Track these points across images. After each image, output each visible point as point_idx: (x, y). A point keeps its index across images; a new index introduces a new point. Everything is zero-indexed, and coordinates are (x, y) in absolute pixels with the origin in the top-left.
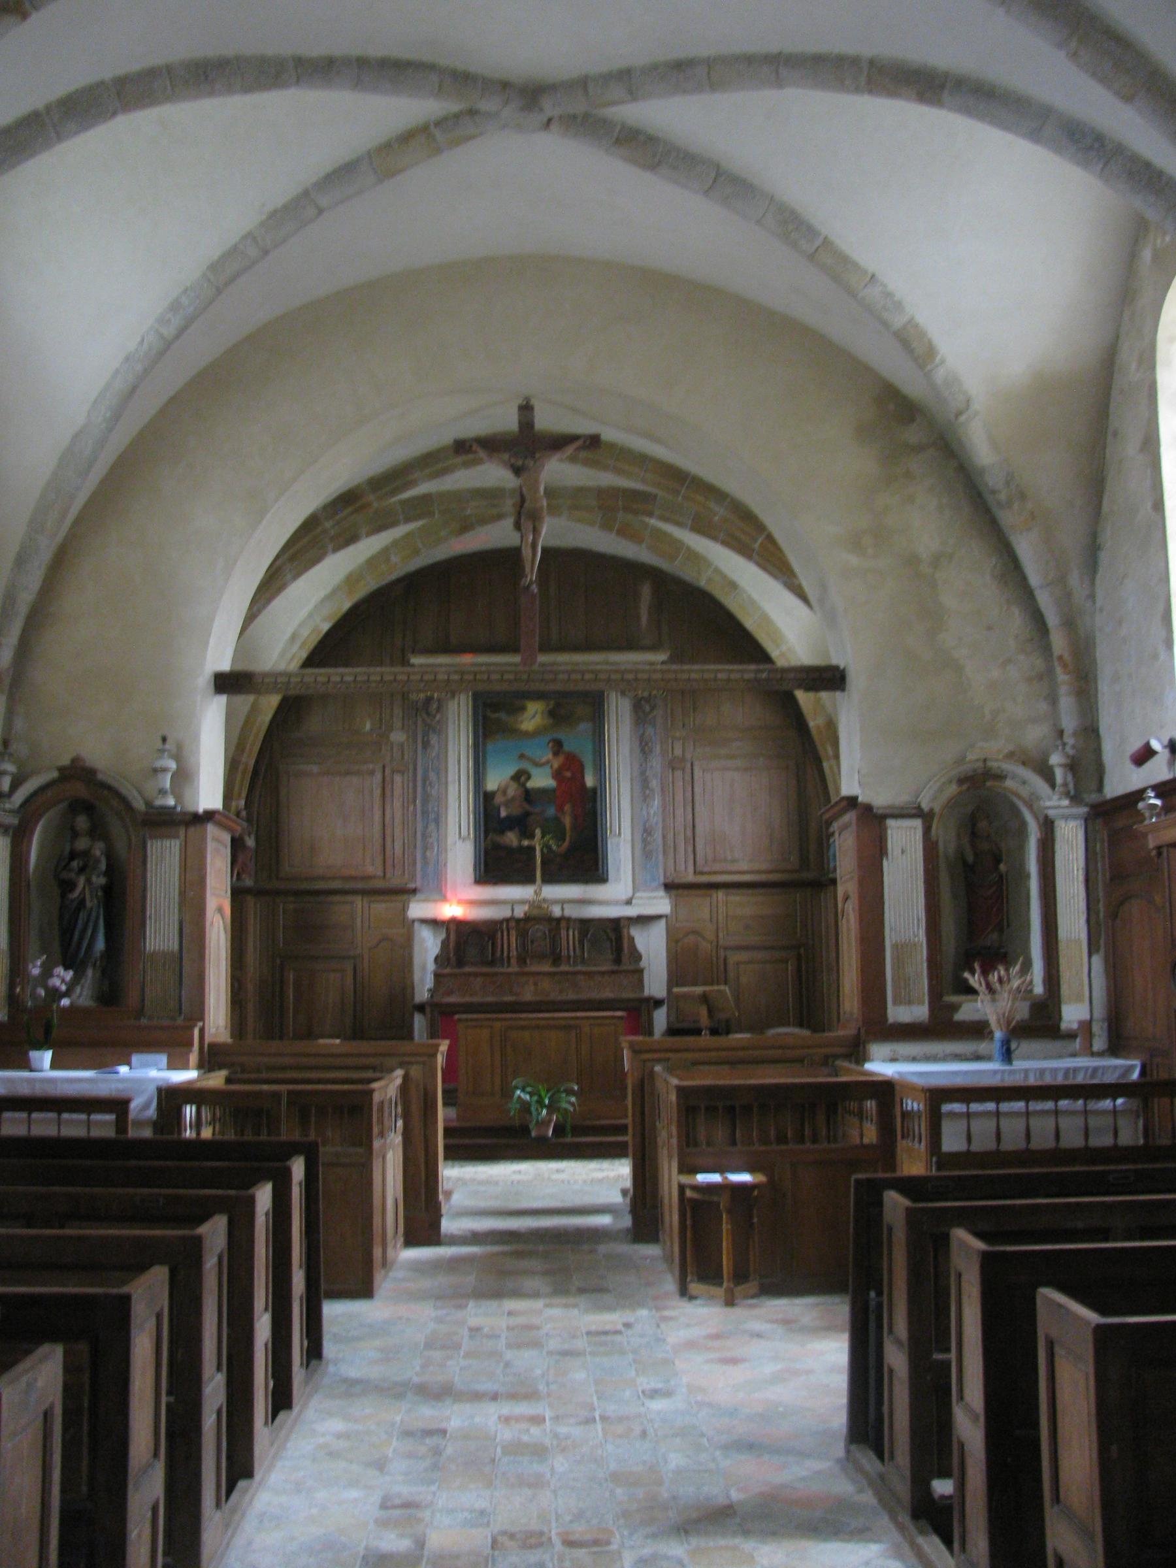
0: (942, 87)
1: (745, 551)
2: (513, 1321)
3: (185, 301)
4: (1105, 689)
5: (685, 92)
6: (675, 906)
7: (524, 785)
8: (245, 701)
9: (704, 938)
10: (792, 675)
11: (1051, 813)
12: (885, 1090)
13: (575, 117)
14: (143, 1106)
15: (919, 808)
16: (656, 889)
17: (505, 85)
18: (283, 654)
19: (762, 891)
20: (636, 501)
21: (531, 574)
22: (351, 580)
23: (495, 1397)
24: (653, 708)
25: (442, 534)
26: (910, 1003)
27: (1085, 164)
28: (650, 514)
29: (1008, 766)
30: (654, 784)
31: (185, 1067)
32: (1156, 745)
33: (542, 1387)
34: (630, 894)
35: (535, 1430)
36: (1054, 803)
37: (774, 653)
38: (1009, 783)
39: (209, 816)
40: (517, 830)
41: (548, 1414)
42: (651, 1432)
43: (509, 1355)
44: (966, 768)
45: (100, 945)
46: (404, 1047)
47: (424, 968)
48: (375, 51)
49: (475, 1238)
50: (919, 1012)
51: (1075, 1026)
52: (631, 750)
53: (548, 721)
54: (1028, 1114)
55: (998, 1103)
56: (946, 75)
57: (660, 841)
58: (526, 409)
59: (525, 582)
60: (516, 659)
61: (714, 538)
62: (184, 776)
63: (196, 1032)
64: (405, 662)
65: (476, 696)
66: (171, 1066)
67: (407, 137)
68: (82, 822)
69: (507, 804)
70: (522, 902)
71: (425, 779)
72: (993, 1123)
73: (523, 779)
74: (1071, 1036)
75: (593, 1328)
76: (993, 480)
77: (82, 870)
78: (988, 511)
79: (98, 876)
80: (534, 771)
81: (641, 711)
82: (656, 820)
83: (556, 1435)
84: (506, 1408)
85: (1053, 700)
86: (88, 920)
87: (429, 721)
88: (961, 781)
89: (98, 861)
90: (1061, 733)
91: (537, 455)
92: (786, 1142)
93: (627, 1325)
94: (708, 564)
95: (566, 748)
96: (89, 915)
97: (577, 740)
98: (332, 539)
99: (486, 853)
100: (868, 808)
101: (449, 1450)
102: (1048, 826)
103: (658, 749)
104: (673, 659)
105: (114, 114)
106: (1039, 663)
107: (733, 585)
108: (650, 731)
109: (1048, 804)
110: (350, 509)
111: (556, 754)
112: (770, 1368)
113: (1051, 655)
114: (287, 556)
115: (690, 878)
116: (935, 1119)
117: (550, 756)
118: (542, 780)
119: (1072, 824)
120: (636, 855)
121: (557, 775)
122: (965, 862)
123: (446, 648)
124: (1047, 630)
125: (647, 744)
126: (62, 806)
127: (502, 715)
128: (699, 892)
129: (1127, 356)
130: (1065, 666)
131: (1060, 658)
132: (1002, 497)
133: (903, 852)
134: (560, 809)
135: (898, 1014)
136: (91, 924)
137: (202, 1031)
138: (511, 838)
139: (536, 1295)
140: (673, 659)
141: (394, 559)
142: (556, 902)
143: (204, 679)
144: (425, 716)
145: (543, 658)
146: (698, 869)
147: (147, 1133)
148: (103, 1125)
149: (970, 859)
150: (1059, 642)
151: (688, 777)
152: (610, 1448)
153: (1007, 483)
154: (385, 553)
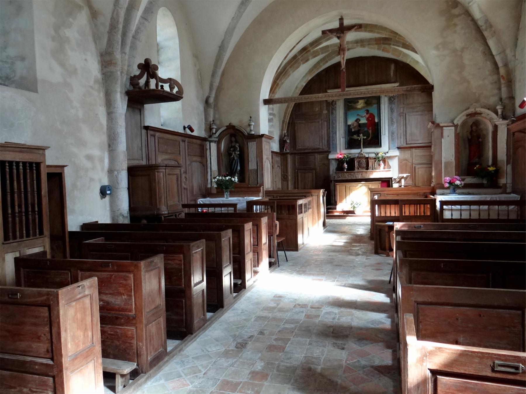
4: (518, 85)
6: (400, 153)
7: (358, 123)
9: (409, 162)
11: (497, 123)
16: (395, 149)
18: (294, 92)
24: (394, 99)
25: (333, 56)
30: (395, 120)
40: (357, 135)
45: (239, 168)
52: (388, 111)
53: (365, 105)
54: (470, 210)
55: (498, 206)
60: (340, 90)
62: (257, 125)
63: (262, 188)
64: (326, 92)
68: (233, 139)
69: (354, 128)
70: (357, 154)
71: (332, 122)
73: (358, 121)
79: (237, 152)
80: (361, 119)
81: (391, 100)
85: (500, 89)
86: (235, 163)
87: (333, 107)
92: (327, 213)
95: (370, 112)
96: (236, 162)
97: (373, 110)
98: (302, 60)
102: (496, 127)
103: (396, 111)
104: (400, 86)
108: (393, 106)
109: (495, 120)
111: (367, 114)
113: (500, 75)
115: (405, 145)
117: (365, 114)
118: (363, 121)
119: (503, 126)
120: (143, 151)
121: (368, 119)
122: (468, 139)
124: (499, 68)
125: (392, 110)
126: (229, 135)
128: (408, 149)
133: (448, 136)
134: (368, 128)
136: (236, 164)
137: (263, 188)
138: (355, 137)
140: (400, 86)
144: (331, 106)
145: (347, 89)
146: (407, 143)
148: (231, 210)
149: (470, 138)
150: (502, 71)
151: (404, 118)
153: (486, 23)
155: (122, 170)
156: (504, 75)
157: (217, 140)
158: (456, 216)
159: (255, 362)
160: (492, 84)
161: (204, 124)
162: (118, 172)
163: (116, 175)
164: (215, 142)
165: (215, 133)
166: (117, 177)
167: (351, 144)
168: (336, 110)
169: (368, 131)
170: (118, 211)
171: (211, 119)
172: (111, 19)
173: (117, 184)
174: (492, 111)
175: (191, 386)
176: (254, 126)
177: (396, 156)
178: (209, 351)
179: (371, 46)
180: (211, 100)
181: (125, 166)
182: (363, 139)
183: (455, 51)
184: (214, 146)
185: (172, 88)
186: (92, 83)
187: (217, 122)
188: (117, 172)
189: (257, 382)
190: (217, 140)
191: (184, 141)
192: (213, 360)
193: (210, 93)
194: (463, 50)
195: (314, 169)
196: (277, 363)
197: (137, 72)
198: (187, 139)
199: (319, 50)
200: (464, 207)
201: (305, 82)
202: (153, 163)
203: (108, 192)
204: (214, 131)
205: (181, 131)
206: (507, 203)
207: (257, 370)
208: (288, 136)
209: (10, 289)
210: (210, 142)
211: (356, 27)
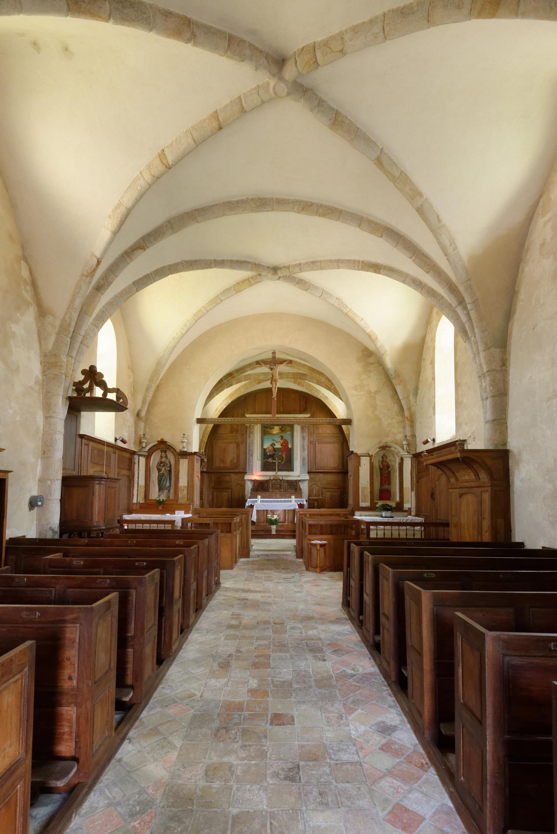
0: (380, 268)
1: (329, 389)
2: (266, 575)
3: (188, 324)
4: (418, 425)
5: (314, 270)
8: (204, 426)
10: (338, 421)
11: (403, 456)
12: (358, 522)
13: (286, 276)
14: (179, 524)
15: (369, 454)
16: (305, 473)
17: (268, 267)
19: (337, 474)
20: (302, 376)
21: (275, 395)
22: (231, 395)
23: (260, 592)
26: (365, 502)
27: (416, 290)
28: (306, 380)
29: (392, 444)
31: (189, 513)
32: (429, 440)
33: (271, 590)
34: (299, 474)
35: (269, 599)
36: (403, 453)
37: (337, 415)
38: (392, 449)
39: (195, 453)
41: (272, 596)
42: (296, 600)
43: (264, 583)
44: (381, 445)
46: (242, 510)
47: (248, 491)
48: (235, 258)
49: (258, 556)
50: (368, 504)
51: (407, 509)
56: (382, 265)
57: (307, 462)
58: (274, 353)
59: (273, 397)
61: (322, 386)
62: (189, 443)
63: (191, 505)
65: (262, 425)
66: (185, 513)
67: (244, 281)
69: (269, 452)
71: (249, 445)
72: (383, 531)
74: (406, 511)
75: (285, 577)
76: (391, 372)
77: (164, 466)
78: (390, 380)
82: (306, 456)
83: (274, 600)
84: (262, 595)
88: (380, 448)
89: (167, 464)
90: (406, 436)
91: (277, 365)
93: (293, 577)
94: (321, 392)
95: (284, 438)
97: (287, 436)
99: (264, 463)
100: (356, 454)
101: (249, 603)
102: (402, 459)
105: (168, 275)
106: (401, 419)
107: (327, 398)
110: (230, 378)
111: (281, 439)
112: (326, 587)
114: (215, 389)
115: (314, 470)
116: (368, 530)
118: (278, 446)
119: (408, 459)
121: (282, 445)
123: (255, 413)
127: (268, 430)
129: (428, 338)
130: (408, 419)
131: (407, 417)
132: (393, 376)
134: (282, 453)
135: (362, 504)
138: (270, 460)
139: (271, 569)
141: (242, 390)
142: (281, 476)
143: (194, 420)
145: (277, 416)
147: (179, 528)
148: (168, 527)
149: (381, 467)
150: (407, 413)
152: (286, 603)
153: (395, 373)
154: (239, 388)
155: (57, 480)
156: (408, 417)
157: (147, 454)
158: (380, 535)
159: (247, 680)
160: (398, 423)
161: (133, 437)
162: (51, 482)
163: (49, 485)
164: (144, 456)
165: (145, 448)
166: (50, 488)
167: (266, 467)
168: (253, 434)
169: (282, 455)
170: (47, 524)
171: (142, 433)
172: (62, 320)
173: (49, 495)
174: (400, 446)
175: (193, 711)
176: (187, 443)
177: (307, 480)
178: (194, 674)
179: (289, 379)
180: (143, 414)
181: (60, 477)
182: (278, 463)
183: (369, 392)
184: (142, 460)
185: (118, 398)
186: (32, 384)
187: (147, 436)
188: (50, 482)
189: (259, 699)
190: (147, 454)
191: (115, 453)
192: (202, 682)
193: (143, 406)
194: (376, 392)
195: (228, 489)
196: (269, 679)
197: (81, 377)
198: (117, 451)
199: (243, 377)
200: (394, 528)
201: (224, 405)
202: (84, 475)
203: (39, 503)
204: (144, 445)
205: (112, 441)
206: (413, 524)
207: (253, 687)
208: (205, 455)
209: (173, 587)
210: (140, 455)
211: (286, 363)
